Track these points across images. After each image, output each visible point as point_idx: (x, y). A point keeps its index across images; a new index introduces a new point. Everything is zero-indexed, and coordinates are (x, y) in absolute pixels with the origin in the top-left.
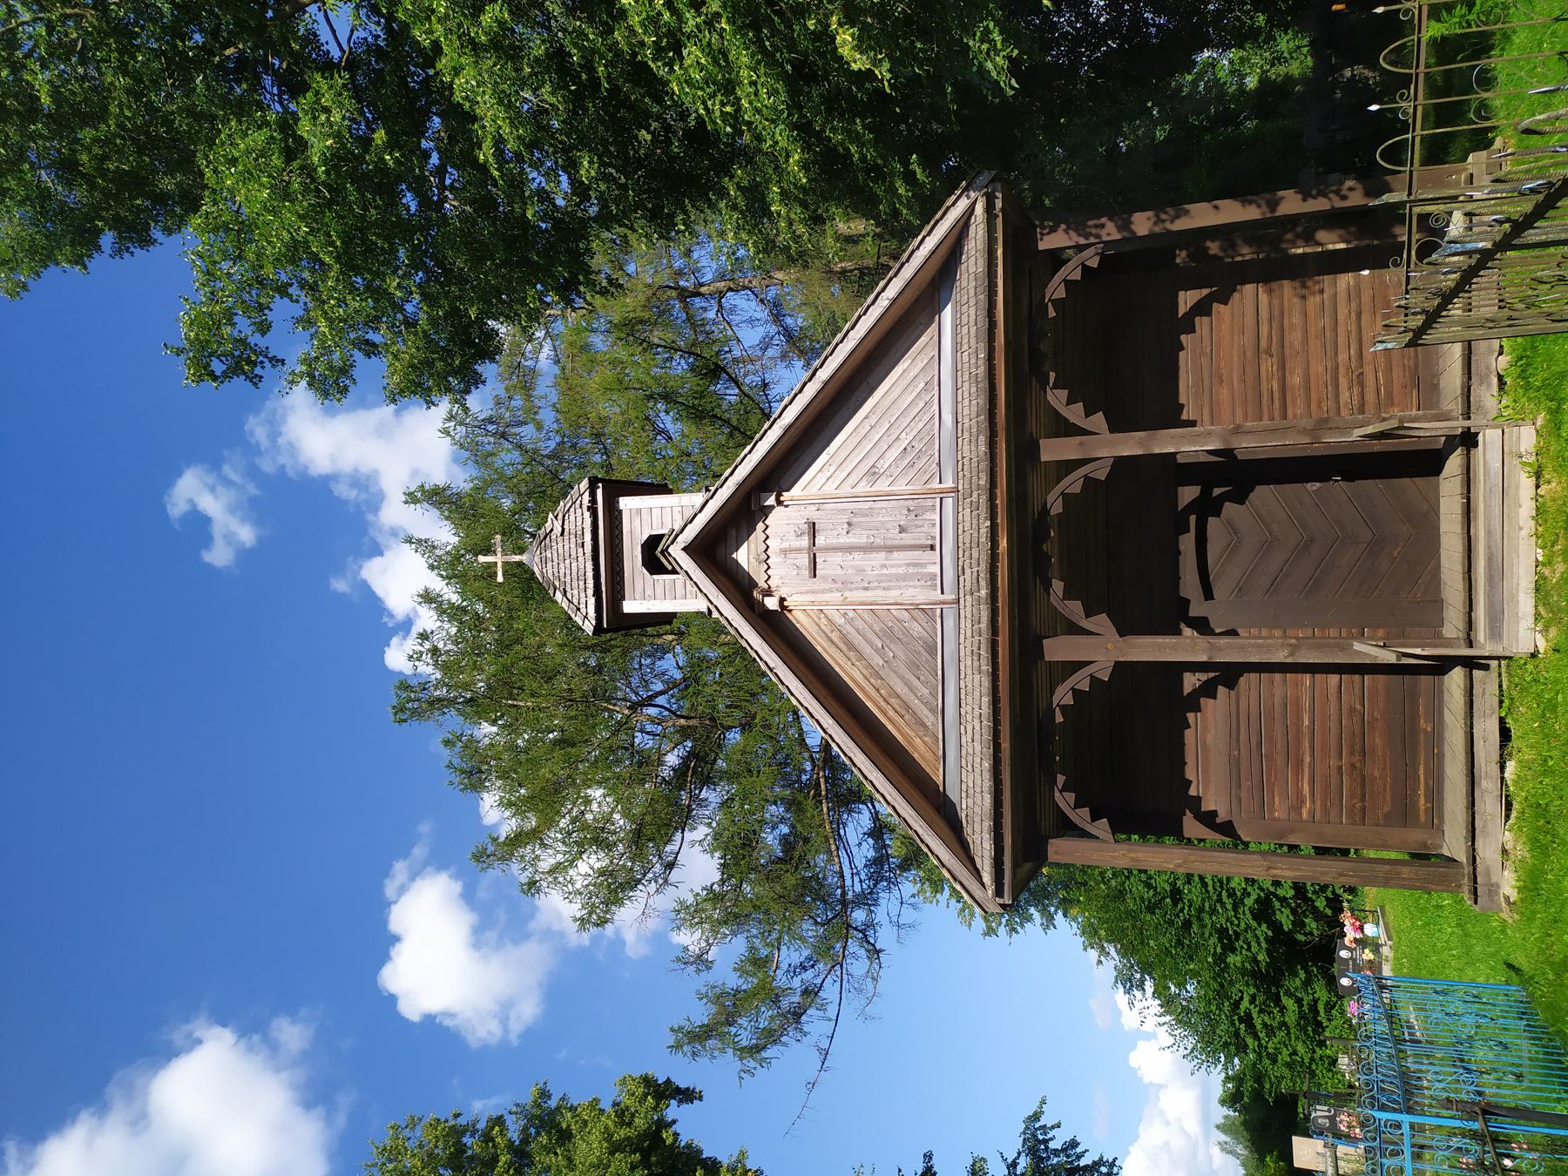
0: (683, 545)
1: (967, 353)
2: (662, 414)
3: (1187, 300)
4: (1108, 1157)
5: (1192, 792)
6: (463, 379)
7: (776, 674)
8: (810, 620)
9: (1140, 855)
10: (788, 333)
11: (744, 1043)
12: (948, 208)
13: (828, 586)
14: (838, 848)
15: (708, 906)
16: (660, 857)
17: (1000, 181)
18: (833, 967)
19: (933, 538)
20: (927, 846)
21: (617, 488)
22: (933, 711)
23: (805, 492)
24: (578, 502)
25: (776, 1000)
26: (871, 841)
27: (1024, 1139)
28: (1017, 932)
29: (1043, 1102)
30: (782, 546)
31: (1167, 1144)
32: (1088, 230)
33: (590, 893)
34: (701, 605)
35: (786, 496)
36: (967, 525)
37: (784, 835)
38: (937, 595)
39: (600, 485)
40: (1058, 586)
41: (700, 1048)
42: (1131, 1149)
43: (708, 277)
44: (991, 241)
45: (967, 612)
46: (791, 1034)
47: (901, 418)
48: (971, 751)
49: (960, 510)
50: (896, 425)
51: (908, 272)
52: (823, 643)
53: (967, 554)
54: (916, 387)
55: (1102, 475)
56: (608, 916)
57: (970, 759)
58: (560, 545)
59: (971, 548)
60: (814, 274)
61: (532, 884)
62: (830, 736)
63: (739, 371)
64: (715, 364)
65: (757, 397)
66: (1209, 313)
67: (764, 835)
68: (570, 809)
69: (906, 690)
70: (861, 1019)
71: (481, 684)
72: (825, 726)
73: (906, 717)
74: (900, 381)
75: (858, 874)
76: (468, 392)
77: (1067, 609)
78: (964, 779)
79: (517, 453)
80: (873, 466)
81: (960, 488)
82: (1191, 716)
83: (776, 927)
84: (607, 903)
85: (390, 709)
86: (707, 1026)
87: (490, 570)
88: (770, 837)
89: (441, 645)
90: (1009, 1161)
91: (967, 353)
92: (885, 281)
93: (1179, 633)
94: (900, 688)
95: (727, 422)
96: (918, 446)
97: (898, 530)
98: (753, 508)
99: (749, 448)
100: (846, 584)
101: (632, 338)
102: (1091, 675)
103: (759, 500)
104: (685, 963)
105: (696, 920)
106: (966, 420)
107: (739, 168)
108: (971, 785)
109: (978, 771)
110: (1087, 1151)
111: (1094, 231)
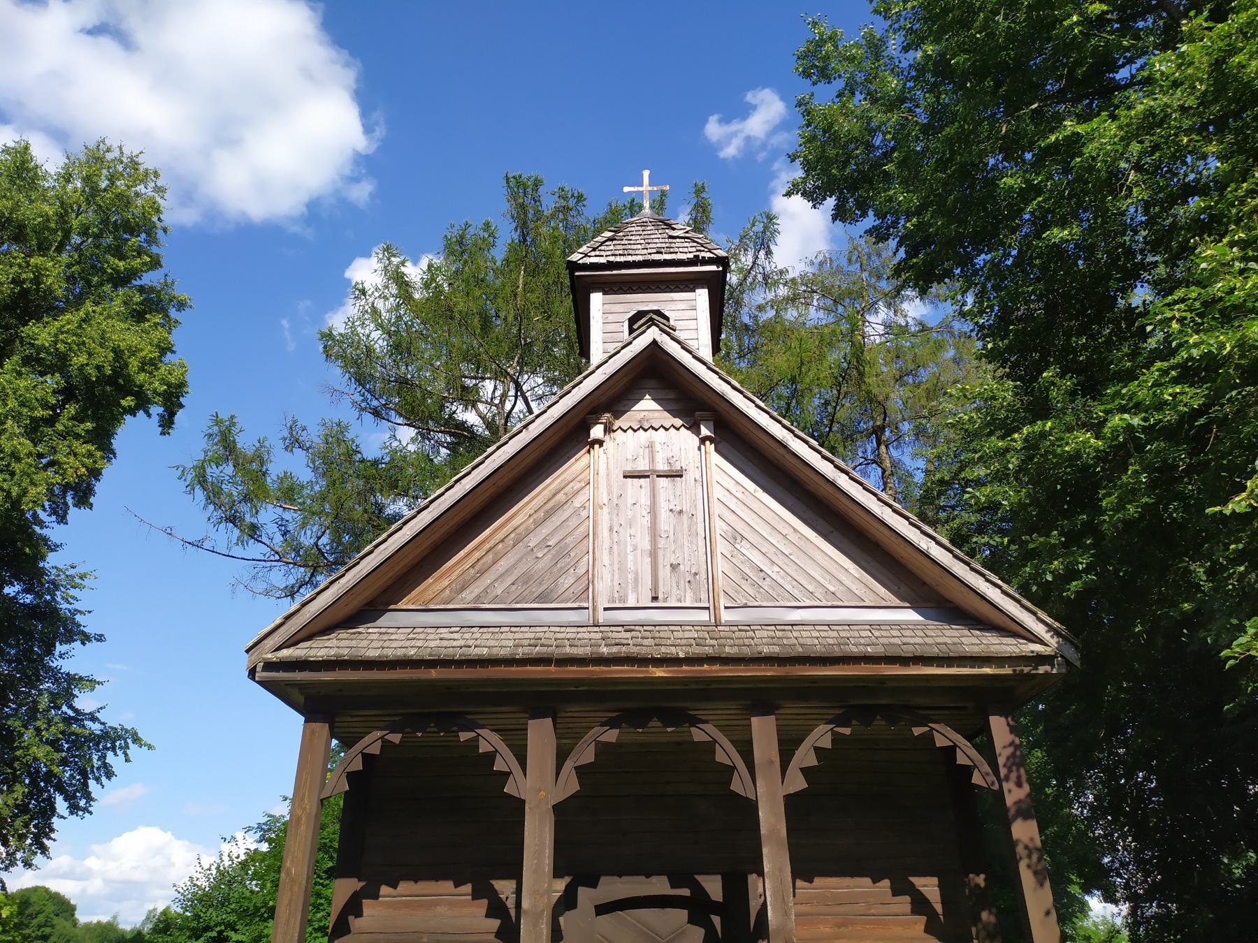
0: (659, 339)
3: (929, 887)
4: (94, 807)
5: (385, 890)
7: (521, 431)
8: (578, 472)
9: (303, 828)
11: (209, 470)
12: (1034, 614)
15: (343, 449)
17: (1069, 672)
21: (716, 286)
22: (478, 598)
23: (714, 467)
24: (703, 249)
25: (246, 498)
27: (116, 729)
29: (150, 747)
31: (173, 865)
32: (1014, 768)
34: (596, 355)
35: (710, 447)
36: (680, 635)
38: (603, 602)
39: (721, 269)
40: (611, 736)
41: (216, 440)
42: (170, 833)
43: (894, 453)
45: (584, 634)
46: (215, 513)
47: (795, 567)
49: (696, 628)
50: (786, 560)
51: (959, 569)
52: (553, 486)
54: (830, 582)
55: (736, 786)
59: (654, 638)
66: (915, 911)
69: (501, 570)
70: (233, 581)
72: (463, 481)
77: (585, 745)
80: (743, 537)
81: (720, 628)
82: (468, 888)
85: (519, 173)
86: (234, 447)
90: (97, 715)
91: (871, 635)
93: (557, 874)
94: (503, 565)
96: (766, 585)
102: (511, 772)
103: (705, 420)
104: (291, 427)
106: (795, 634)
108: (393, 637)
109: (408, 643)
110: (103, 787)
111: (1013, 776)
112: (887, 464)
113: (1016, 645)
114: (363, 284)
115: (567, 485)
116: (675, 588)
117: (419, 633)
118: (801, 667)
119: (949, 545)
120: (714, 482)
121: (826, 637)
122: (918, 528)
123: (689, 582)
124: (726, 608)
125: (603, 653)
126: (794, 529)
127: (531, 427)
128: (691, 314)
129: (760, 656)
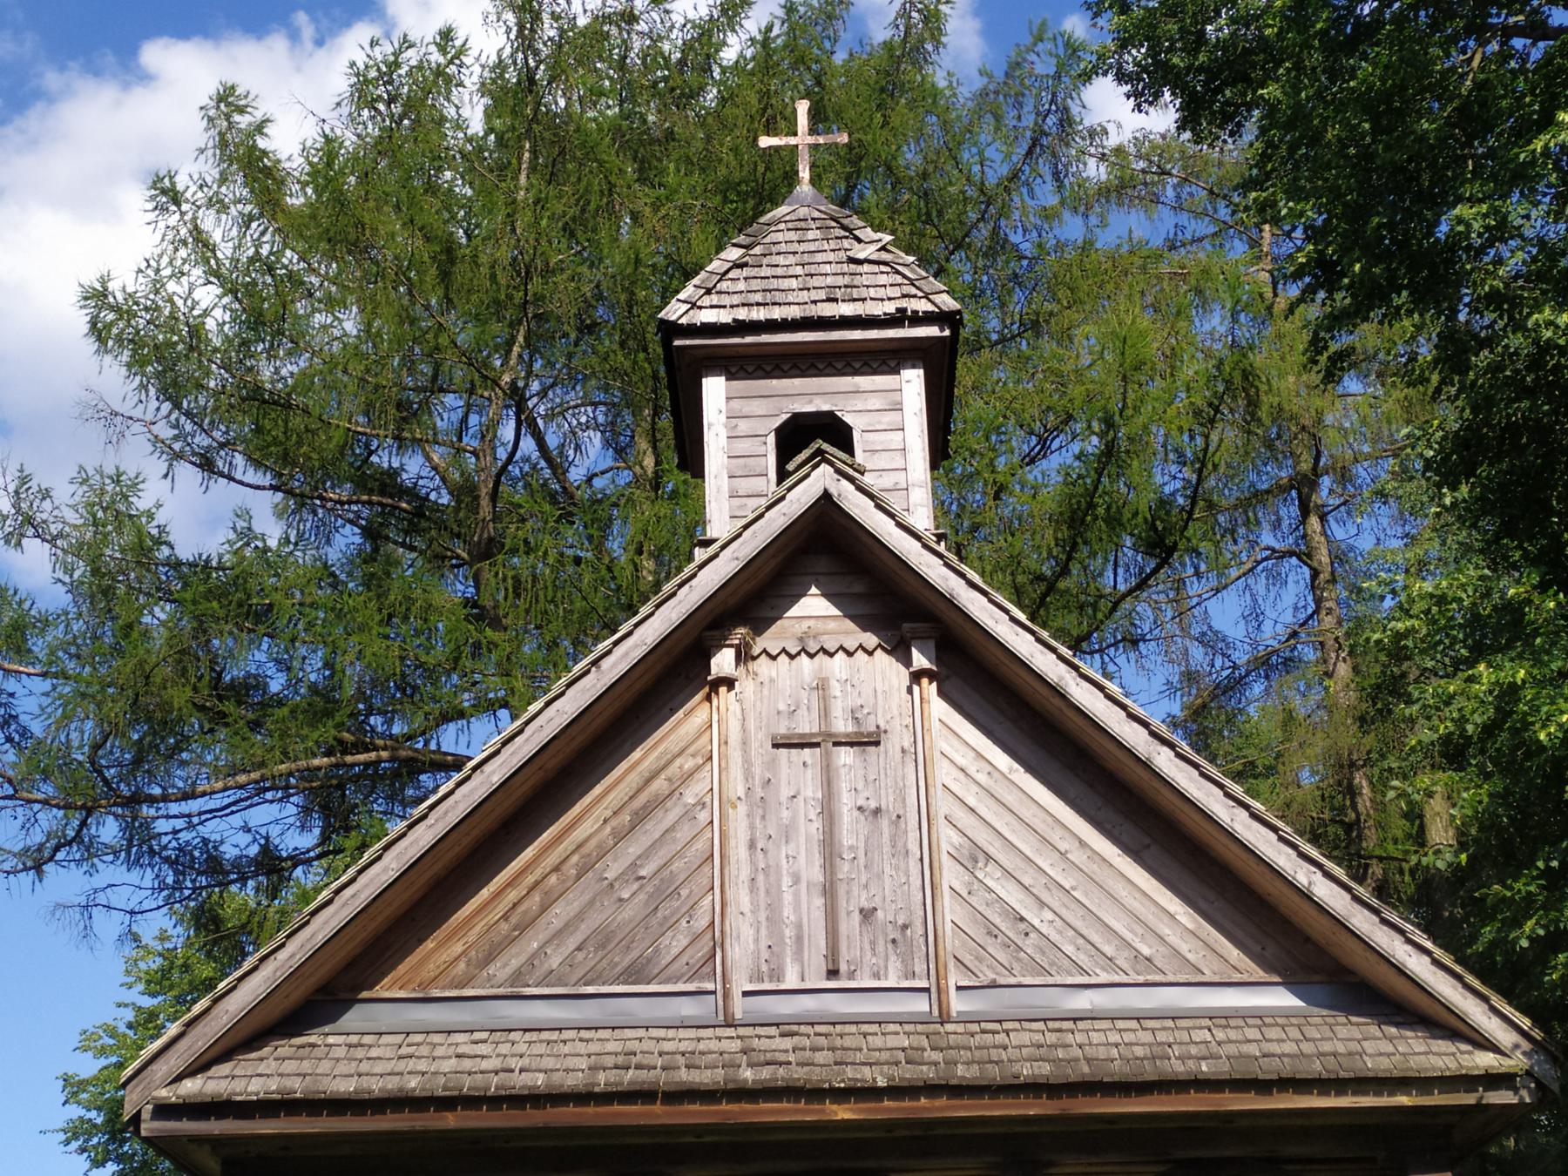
0: (833, 491)
1: (1209, 1038)
2: (1076, 447)
6: (1145, 69)
7: (588, 672)
8: (690, 738)
10: (1235, 685)
12: (1485, 999)
13: (757, 770)
14: (241, 787)
15: (128, 538)
16: (222, 446)
18: (10, 781)
19: (851, 975)
20: (255, 969)
22: (517, 977)
23: (936, 725)
24: (914, 291)
26: (254, 850)
28: (67, 1142)
30: (833, 683)
33: (158, 309)
34: (719, 524)
35: (931, 689)
36: (877, 1041)
37: (266, 685)
39: (947, 333)
43: (1339, 533)
44: (1424, 1083)
47: (1082, 912)
48: (440, 1051)
49: (908, 1028)
50: (1066, 900)
52: (646, 764)
53: (822, 1041)
56: (110, 343)
57: (424, 1050)
58: (831, 257)
59: (832, 1049)
60: (1348, 737)
61: (175, 198)
62: (468, 778)
63: (1159, 591)
64: (1174, 548)
65: (1110, 626)
67: (265, 646)
68: (321, 274)
69: (557, 924)
71: (562, 103)
72: (488, 768)
73: (504, 927)
74: (1153, 909)
75: (191, 826)
76: (1121, 78)
78: (385, 1039)
79: (1004, 170)
80: (988, 857)
81: (949, 1027)
83: (88, 669)
84: (136, 342)
87: (779, 121)
88: (260, 656)
89: (642, 26)
91: (1209, 1038)
92: (1345, 879)
94: (560, 913)
95: (1065, 571)
96: (1029, 945)
97: (865, 904)
98: (906, 626)
99: (1022, 617)
100: (761, 805)
101: (1221, 388)
103: (919, 637)
104: (17, 492)
105: (100, 514)
106: (1080, 1038)
107: (1559, 604)
108: (374, 1053)
109: (402, 1066)
112: (1323, 557)
113: (1453, 1054)
114: (171, 178)
115: (670, 762)
116: (869, 953)
117: (418, 1045)
118: (1087, 1099)
119: (1345, 879)
120: (937, 755)
121: (1131, 1044)
122: (1294, 846)
123: (894, 941)
124: (959, 988)
125: (746, 1080)
126: (1081, 841)
127: (606, 663)
128: (889, 419)
129: (1016, 1082)
